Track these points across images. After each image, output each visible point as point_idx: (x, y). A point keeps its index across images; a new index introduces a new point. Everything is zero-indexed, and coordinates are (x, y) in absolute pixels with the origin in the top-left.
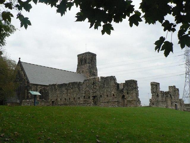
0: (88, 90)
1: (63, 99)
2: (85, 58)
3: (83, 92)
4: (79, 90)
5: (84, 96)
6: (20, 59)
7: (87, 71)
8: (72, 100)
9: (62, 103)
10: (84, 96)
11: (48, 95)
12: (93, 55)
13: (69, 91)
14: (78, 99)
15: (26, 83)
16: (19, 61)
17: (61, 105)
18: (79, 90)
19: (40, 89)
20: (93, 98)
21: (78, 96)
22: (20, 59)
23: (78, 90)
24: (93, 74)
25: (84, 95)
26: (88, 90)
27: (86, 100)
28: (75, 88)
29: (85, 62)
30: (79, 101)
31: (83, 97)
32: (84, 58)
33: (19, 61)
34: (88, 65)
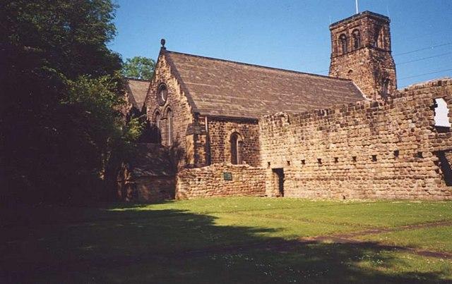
0: (413, 130)
1: (311, 162)
2: (356, 33)
3: (391, 137)
4: (374, 131)
5: (396, 153)
6: (163, 42)
7: (364, 69)
8: (345, 164)
9: (309, 173)
10: (396, 153)
11: (256, 147)
12: (377, 20)
13: (332, 134)
14: (369, 161)
15: (188, 116)
16: (163, 48)
17: (305, 180)
18: (374, 131)
19: (233, 130)
20: (436, 158)
21: (370, 151)
22: (163, 42)
23: (368, 130)
24: (383, 79)
25: (394, 147)
26: (413, 130)
27: (406, 164)
28: (357, 123)
29: (357, 46)
30: (373, 170)
31: (391, 155)
32: (351, 31)
33: (163, 48)
34: (367, 53)
